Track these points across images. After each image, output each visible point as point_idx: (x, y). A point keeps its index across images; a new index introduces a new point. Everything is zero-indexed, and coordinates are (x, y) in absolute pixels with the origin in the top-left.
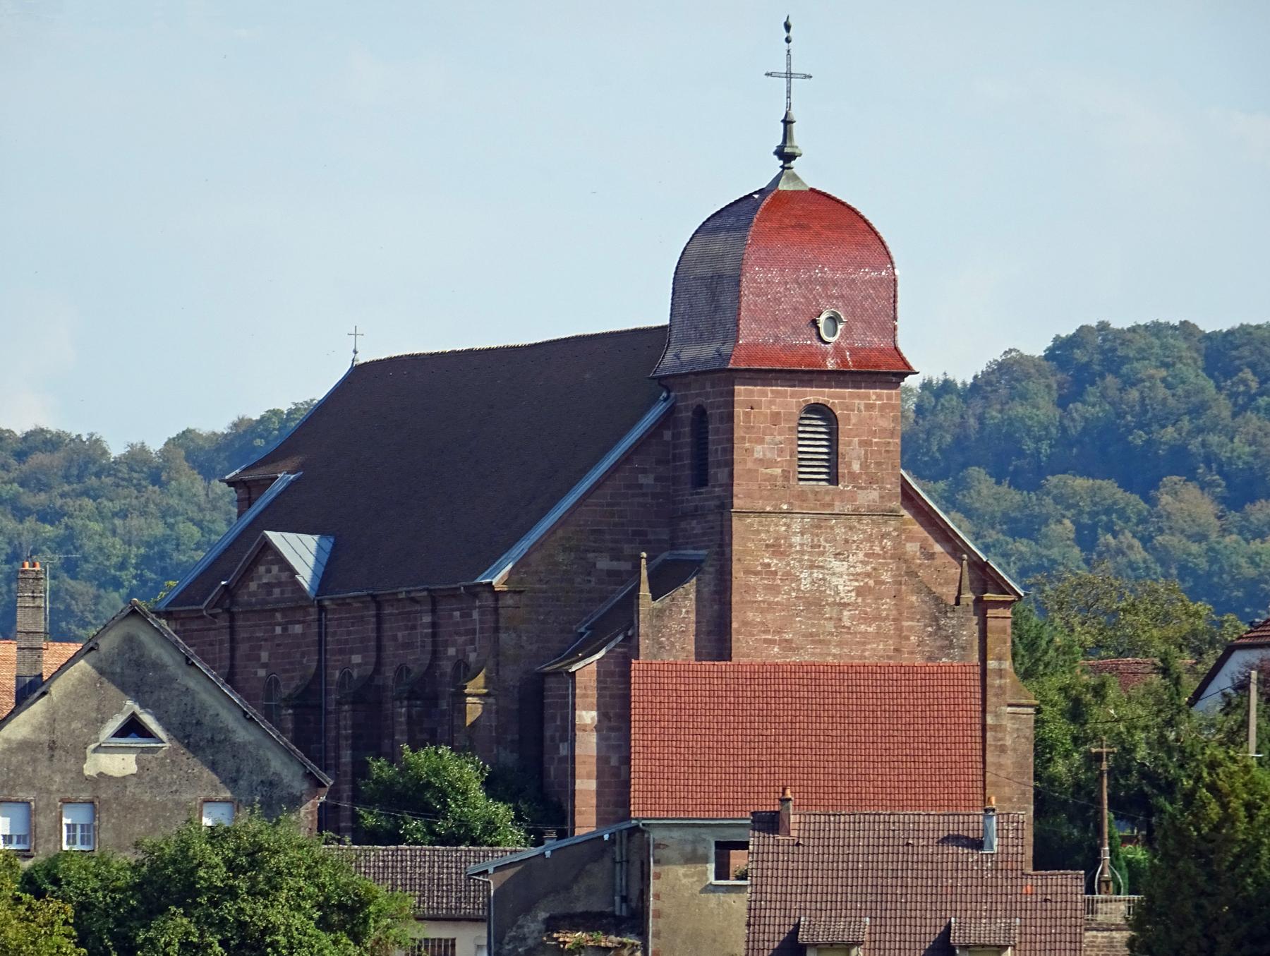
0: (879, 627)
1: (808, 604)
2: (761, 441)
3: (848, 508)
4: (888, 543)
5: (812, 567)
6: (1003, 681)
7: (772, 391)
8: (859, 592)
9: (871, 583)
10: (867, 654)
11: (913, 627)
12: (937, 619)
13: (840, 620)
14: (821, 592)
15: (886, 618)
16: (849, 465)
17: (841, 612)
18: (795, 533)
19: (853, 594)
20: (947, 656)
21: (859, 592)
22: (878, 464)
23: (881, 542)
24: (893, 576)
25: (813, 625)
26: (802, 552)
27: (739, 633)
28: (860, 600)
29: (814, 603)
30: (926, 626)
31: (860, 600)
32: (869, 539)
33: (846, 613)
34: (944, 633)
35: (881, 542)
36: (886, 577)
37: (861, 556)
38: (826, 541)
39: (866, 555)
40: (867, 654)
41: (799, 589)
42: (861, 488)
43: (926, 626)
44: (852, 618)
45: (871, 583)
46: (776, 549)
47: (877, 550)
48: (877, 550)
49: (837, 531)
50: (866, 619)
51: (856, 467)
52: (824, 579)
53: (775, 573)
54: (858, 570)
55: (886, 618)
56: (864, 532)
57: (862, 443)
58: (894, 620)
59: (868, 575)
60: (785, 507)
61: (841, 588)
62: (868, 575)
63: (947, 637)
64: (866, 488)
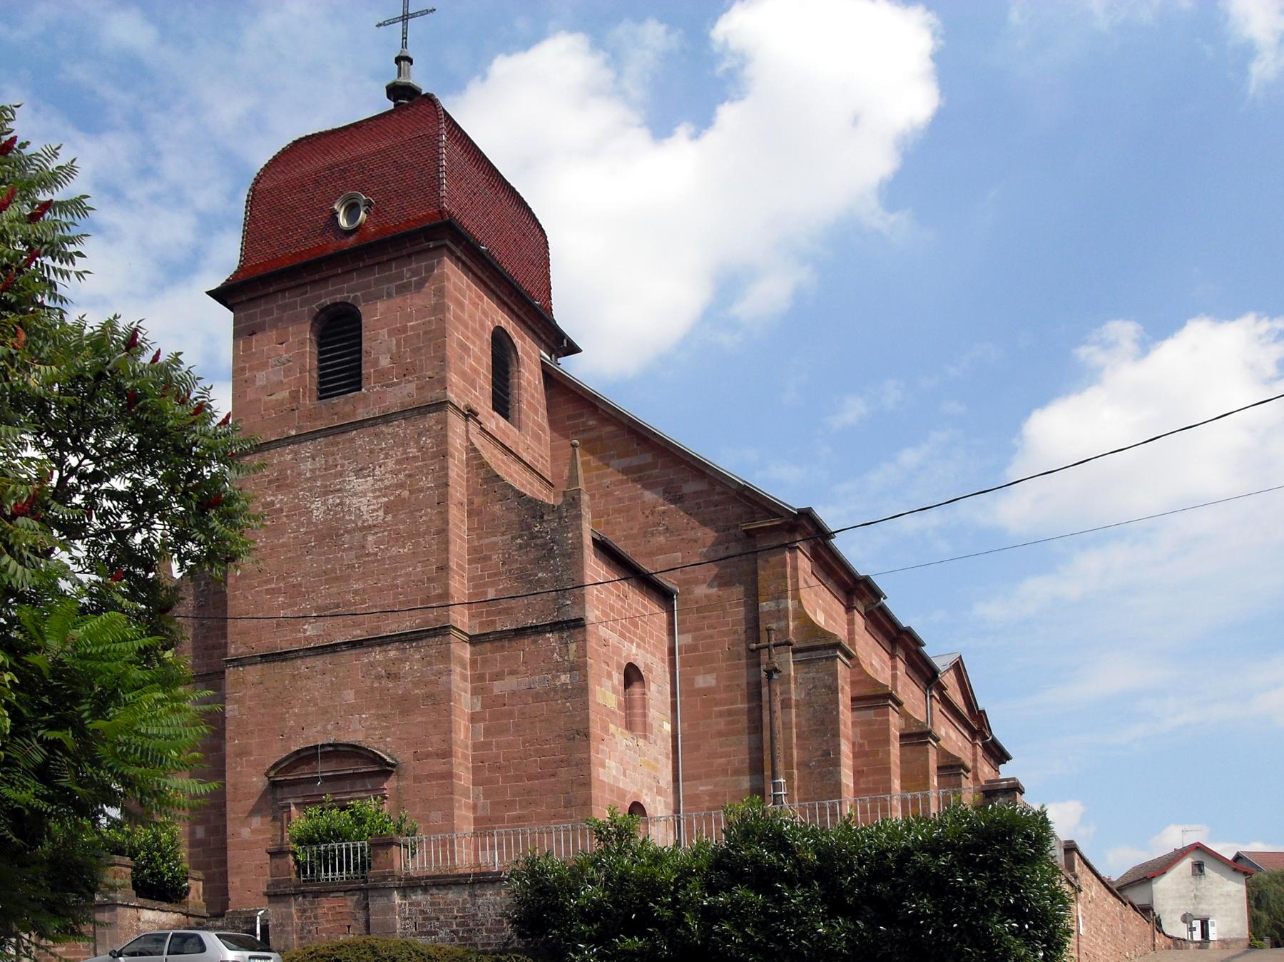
0: (416, 544)
1: (321, 538)
2: (263, 366)
3: (376, 412)
4: (426, 441)
5: (326, 492)
6: (782, 623)
7: (279, 307)
8: (388, 508)
9: (406, 494)
10: (399, 581)
11: (496, 544)
12: (529, 528)
13: (364, 547)
14: (337, 520)
15: (427, 532)
16: (377, 361)
17: (364, 538)
18: (305, 459)
19: (381, 513)
20: (544, 569)
21: (388, 508)
22: (416, 351)
23: (418, 442)
24: (435, 480)
25: (328, 561)
26: (314, 479)
27: (235, 588)
28: (389, 518)
29: (330, 534)
30: (513, 538)
31: (389, 518)
32: (404, 444)
33: (370, 538)
34: (539, 541)
35: (418, 442)
36: (426, 482)
37: (391, 464)
38: (344, 458)
39: (398, 462)
40: (399, 581)
41: (310, 522)
42: (392, 385)
43: (513, 538)
44: (378, 543)
45: (406, 494)
46: (281, 484)
47: (413, 451)
48: (413, 451)
49: (359, 442)
50: (398, 539)
51: (385, 362)
52: (341, 504)
53: (281, 510)
54: (386, 482)
55: (427, 532)
56: (394, 436)
57: (390, 333)
58: (438, 533)
59: (401, 486)
60: (293, 433)
61: (364, 508)
62: (401, 486)
63: (543, 546)
64: (398, 384)
